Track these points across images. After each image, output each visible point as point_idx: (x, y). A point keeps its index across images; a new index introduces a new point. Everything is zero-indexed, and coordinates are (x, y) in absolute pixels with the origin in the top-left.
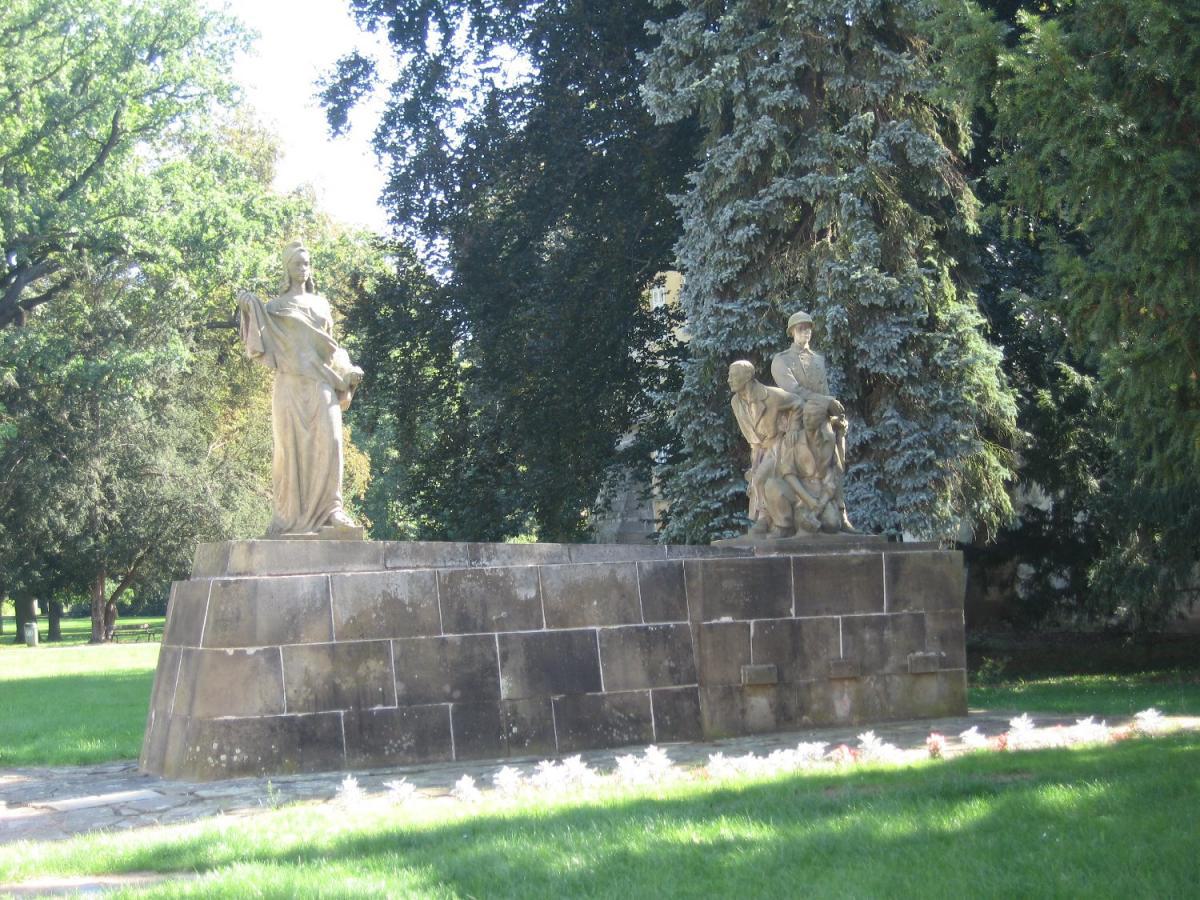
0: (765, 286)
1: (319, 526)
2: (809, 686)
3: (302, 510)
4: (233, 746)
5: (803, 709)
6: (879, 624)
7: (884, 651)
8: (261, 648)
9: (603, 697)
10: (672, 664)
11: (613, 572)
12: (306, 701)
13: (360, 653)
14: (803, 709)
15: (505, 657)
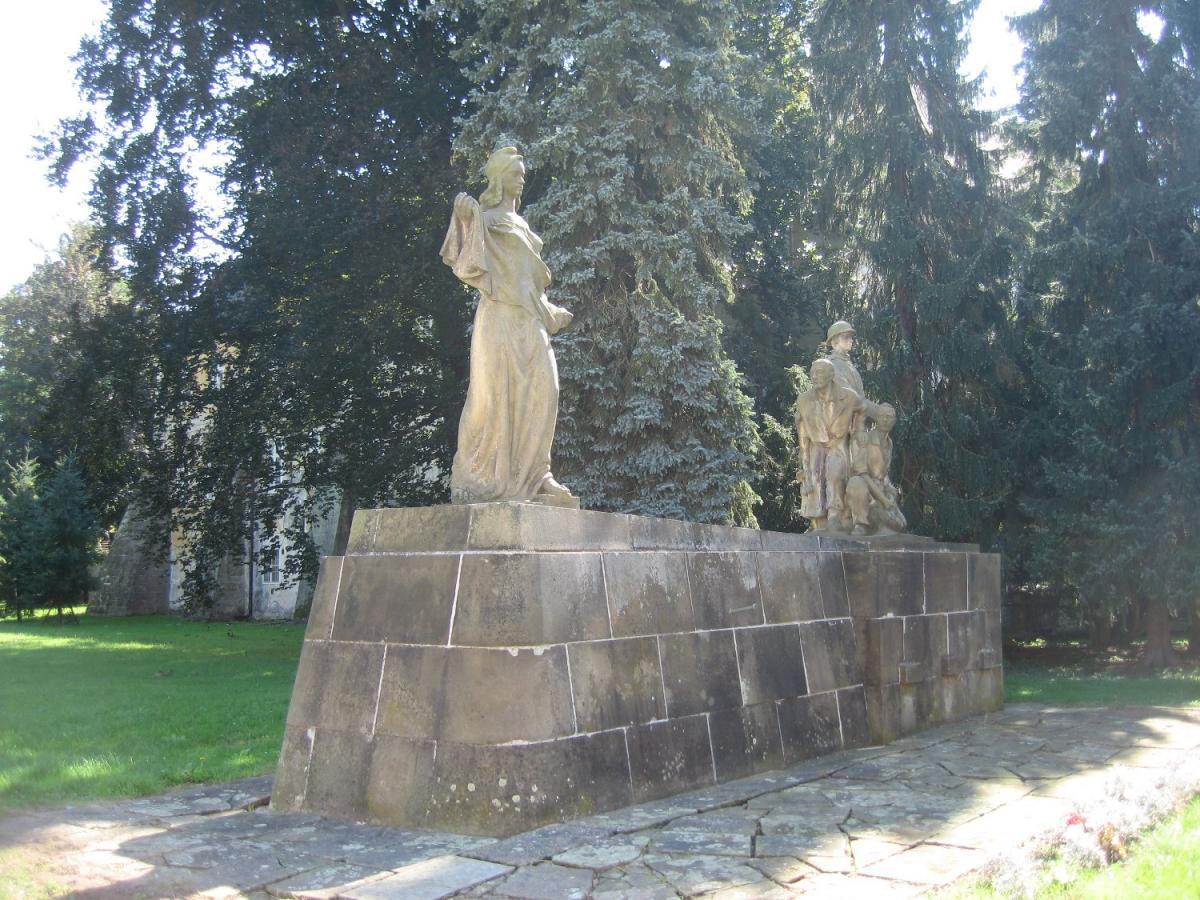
0: (587, 325)
1: (534, 494)
3: (514, 474)
4: (528, 782)
9: (808, 699)
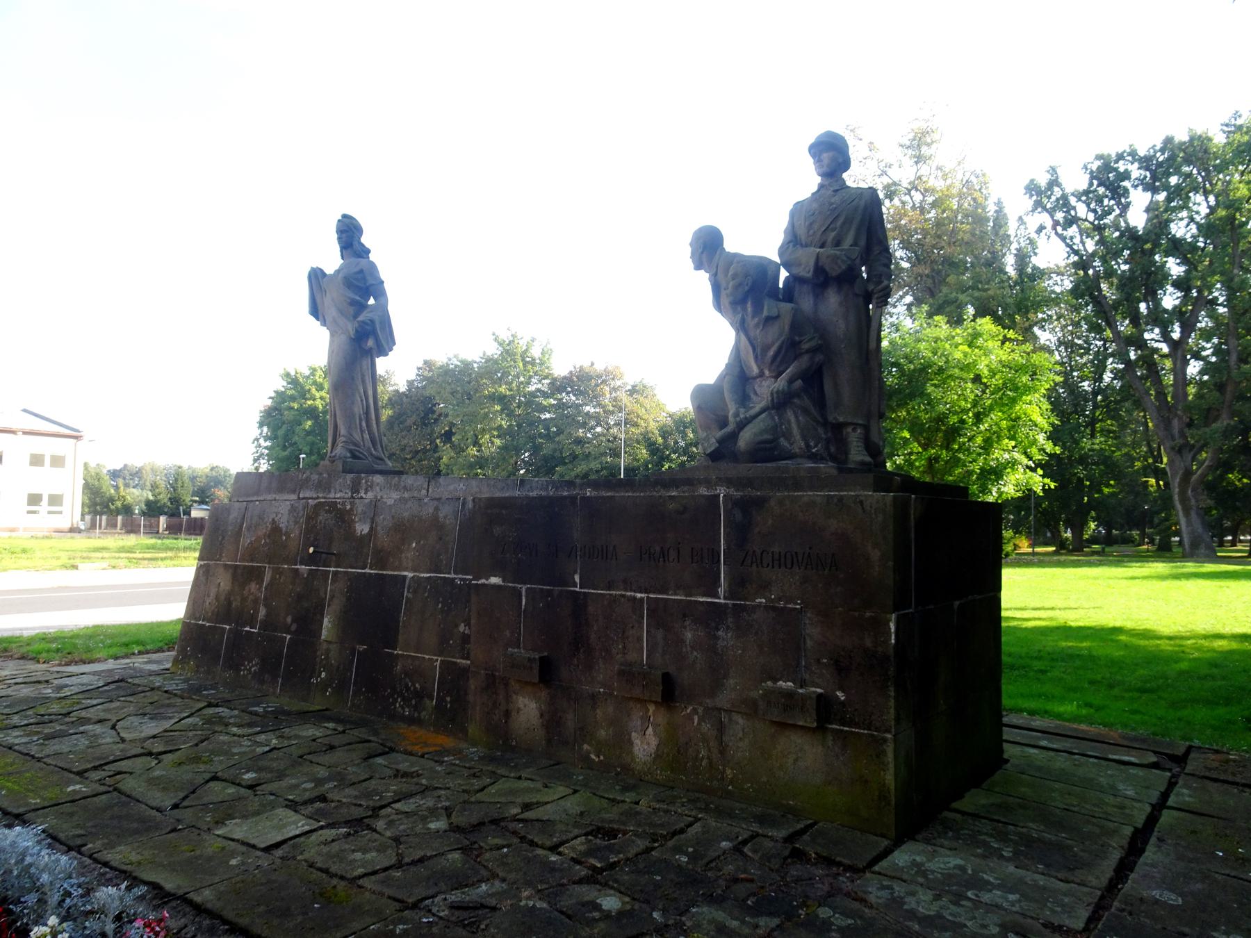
2: (593, 697)
15: (332, 597)
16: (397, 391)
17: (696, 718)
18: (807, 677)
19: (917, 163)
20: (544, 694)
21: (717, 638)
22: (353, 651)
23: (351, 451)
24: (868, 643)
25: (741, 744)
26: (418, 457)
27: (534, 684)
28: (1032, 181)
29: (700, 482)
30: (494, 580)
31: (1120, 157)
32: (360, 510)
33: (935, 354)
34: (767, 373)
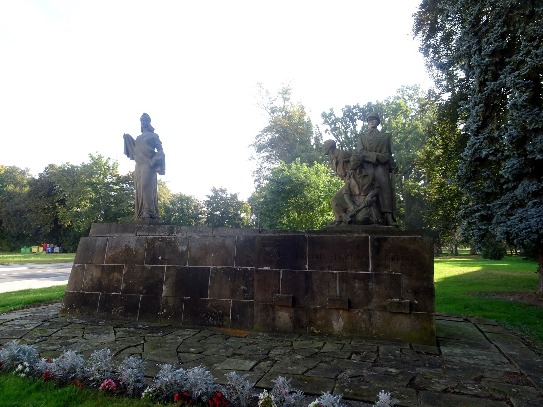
2: (315, 310)
5: (311, 322)
6: (367, 278)
7: (368, 296)
8: (79, 265)
10: (245, 288)
11: (224, 240)
12: (89, 287)
13: (113, 269)
14: (311, 322)
15: (167, 278)
16: (33, 179)
17: (360, 314)
18: (404, 296)
19: (284, 100)
20: (292, 310)
21: (369, 285)
22: (182, 300)
23: (150, 215)
24: (425, 284)
25: (378, 321)
26: (45, 211)
27: (288, 306)
28: (324, 112)
29: (354, 232)
30: (265, 268)
31: (354, 107)
32: (180, 240)
33: (306, 178)
34: (362, 194)
